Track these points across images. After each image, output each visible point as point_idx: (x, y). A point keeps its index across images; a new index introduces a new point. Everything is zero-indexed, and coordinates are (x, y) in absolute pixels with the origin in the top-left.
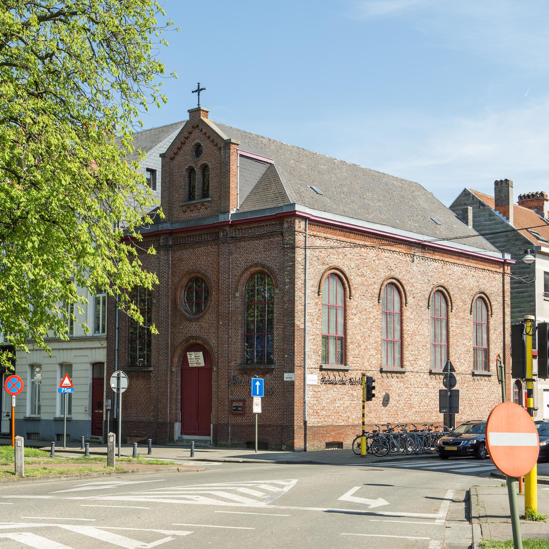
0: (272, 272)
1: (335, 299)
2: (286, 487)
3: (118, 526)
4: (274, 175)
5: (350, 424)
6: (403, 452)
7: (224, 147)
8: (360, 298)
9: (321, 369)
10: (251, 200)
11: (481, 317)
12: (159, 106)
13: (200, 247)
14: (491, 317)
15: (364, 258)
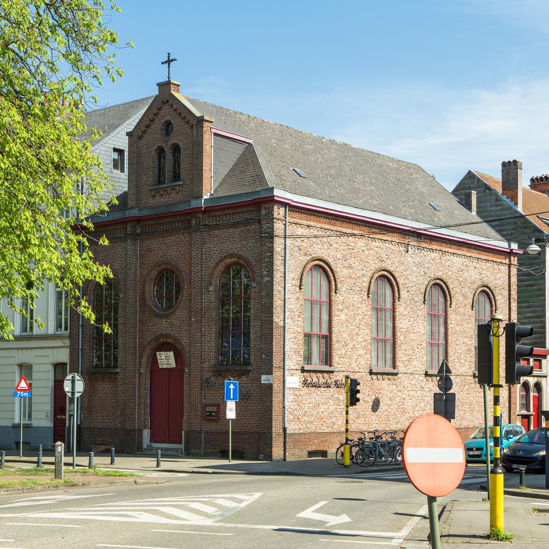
0: (248, 263)
1: (319, 293)
5: (335, 431)
7: (196, 125)
9: (303, 370)
10: (227, 184)
11: (484, 313)
12: (113, 81)
13: (171, 236)
15: (351, 247)
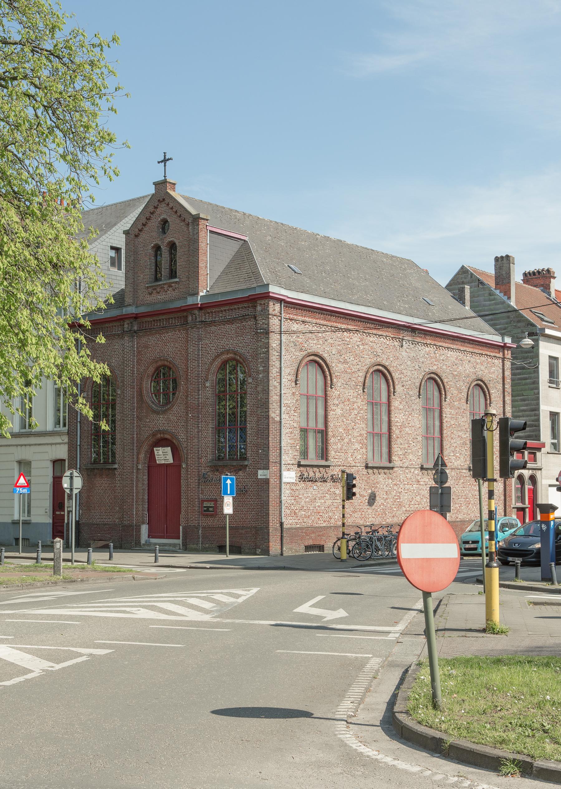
0: (245, 360)
2: (243, 597)
3: (34, 645)
4: (247, 252)
5: (332, 525)
6: (388, 555)
7: (192, 223)
8: (342, 387)
9: (299, 465)
10: (223, 281)
13: (167, 333)
14: (490, 406)
